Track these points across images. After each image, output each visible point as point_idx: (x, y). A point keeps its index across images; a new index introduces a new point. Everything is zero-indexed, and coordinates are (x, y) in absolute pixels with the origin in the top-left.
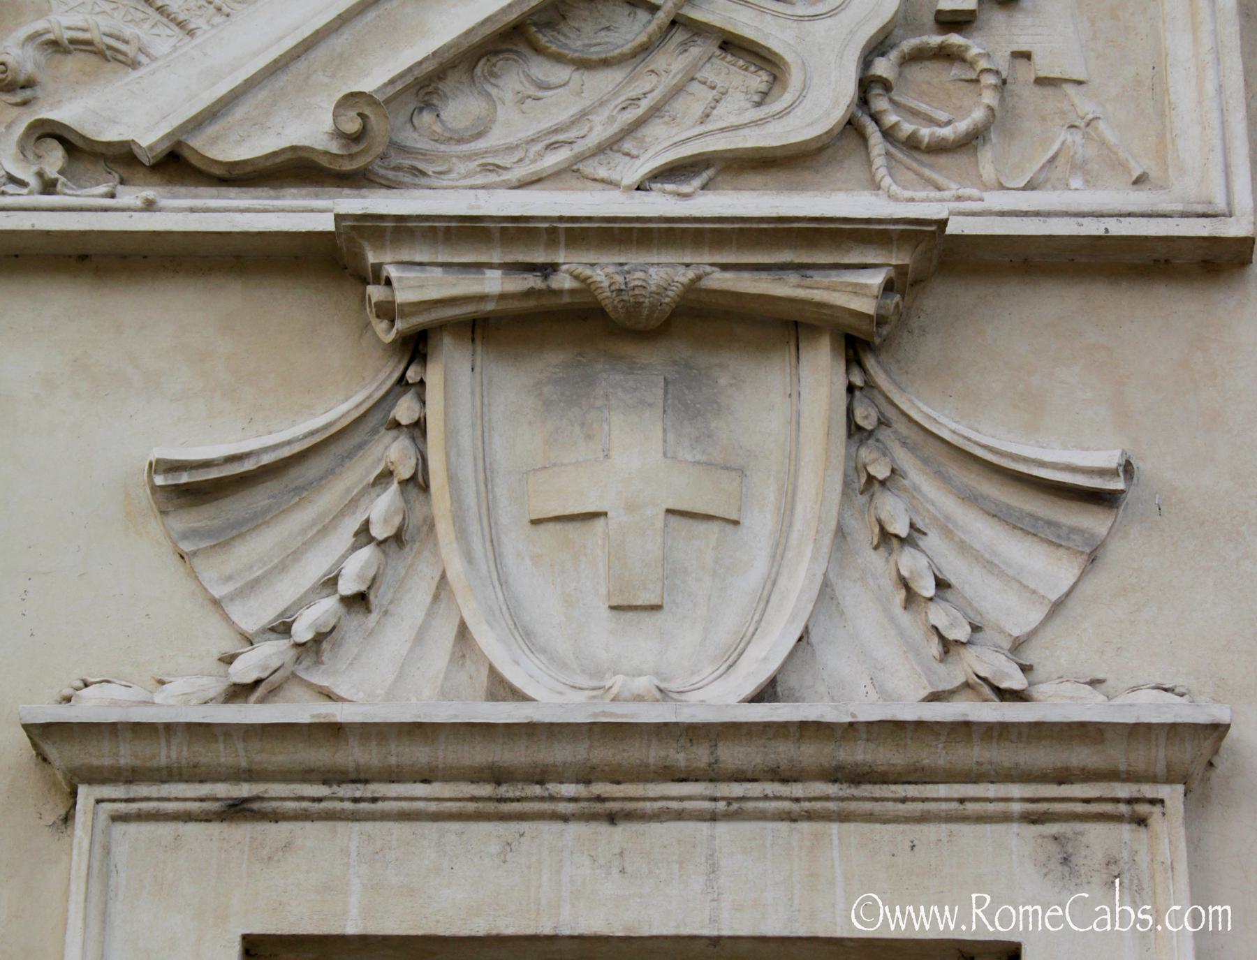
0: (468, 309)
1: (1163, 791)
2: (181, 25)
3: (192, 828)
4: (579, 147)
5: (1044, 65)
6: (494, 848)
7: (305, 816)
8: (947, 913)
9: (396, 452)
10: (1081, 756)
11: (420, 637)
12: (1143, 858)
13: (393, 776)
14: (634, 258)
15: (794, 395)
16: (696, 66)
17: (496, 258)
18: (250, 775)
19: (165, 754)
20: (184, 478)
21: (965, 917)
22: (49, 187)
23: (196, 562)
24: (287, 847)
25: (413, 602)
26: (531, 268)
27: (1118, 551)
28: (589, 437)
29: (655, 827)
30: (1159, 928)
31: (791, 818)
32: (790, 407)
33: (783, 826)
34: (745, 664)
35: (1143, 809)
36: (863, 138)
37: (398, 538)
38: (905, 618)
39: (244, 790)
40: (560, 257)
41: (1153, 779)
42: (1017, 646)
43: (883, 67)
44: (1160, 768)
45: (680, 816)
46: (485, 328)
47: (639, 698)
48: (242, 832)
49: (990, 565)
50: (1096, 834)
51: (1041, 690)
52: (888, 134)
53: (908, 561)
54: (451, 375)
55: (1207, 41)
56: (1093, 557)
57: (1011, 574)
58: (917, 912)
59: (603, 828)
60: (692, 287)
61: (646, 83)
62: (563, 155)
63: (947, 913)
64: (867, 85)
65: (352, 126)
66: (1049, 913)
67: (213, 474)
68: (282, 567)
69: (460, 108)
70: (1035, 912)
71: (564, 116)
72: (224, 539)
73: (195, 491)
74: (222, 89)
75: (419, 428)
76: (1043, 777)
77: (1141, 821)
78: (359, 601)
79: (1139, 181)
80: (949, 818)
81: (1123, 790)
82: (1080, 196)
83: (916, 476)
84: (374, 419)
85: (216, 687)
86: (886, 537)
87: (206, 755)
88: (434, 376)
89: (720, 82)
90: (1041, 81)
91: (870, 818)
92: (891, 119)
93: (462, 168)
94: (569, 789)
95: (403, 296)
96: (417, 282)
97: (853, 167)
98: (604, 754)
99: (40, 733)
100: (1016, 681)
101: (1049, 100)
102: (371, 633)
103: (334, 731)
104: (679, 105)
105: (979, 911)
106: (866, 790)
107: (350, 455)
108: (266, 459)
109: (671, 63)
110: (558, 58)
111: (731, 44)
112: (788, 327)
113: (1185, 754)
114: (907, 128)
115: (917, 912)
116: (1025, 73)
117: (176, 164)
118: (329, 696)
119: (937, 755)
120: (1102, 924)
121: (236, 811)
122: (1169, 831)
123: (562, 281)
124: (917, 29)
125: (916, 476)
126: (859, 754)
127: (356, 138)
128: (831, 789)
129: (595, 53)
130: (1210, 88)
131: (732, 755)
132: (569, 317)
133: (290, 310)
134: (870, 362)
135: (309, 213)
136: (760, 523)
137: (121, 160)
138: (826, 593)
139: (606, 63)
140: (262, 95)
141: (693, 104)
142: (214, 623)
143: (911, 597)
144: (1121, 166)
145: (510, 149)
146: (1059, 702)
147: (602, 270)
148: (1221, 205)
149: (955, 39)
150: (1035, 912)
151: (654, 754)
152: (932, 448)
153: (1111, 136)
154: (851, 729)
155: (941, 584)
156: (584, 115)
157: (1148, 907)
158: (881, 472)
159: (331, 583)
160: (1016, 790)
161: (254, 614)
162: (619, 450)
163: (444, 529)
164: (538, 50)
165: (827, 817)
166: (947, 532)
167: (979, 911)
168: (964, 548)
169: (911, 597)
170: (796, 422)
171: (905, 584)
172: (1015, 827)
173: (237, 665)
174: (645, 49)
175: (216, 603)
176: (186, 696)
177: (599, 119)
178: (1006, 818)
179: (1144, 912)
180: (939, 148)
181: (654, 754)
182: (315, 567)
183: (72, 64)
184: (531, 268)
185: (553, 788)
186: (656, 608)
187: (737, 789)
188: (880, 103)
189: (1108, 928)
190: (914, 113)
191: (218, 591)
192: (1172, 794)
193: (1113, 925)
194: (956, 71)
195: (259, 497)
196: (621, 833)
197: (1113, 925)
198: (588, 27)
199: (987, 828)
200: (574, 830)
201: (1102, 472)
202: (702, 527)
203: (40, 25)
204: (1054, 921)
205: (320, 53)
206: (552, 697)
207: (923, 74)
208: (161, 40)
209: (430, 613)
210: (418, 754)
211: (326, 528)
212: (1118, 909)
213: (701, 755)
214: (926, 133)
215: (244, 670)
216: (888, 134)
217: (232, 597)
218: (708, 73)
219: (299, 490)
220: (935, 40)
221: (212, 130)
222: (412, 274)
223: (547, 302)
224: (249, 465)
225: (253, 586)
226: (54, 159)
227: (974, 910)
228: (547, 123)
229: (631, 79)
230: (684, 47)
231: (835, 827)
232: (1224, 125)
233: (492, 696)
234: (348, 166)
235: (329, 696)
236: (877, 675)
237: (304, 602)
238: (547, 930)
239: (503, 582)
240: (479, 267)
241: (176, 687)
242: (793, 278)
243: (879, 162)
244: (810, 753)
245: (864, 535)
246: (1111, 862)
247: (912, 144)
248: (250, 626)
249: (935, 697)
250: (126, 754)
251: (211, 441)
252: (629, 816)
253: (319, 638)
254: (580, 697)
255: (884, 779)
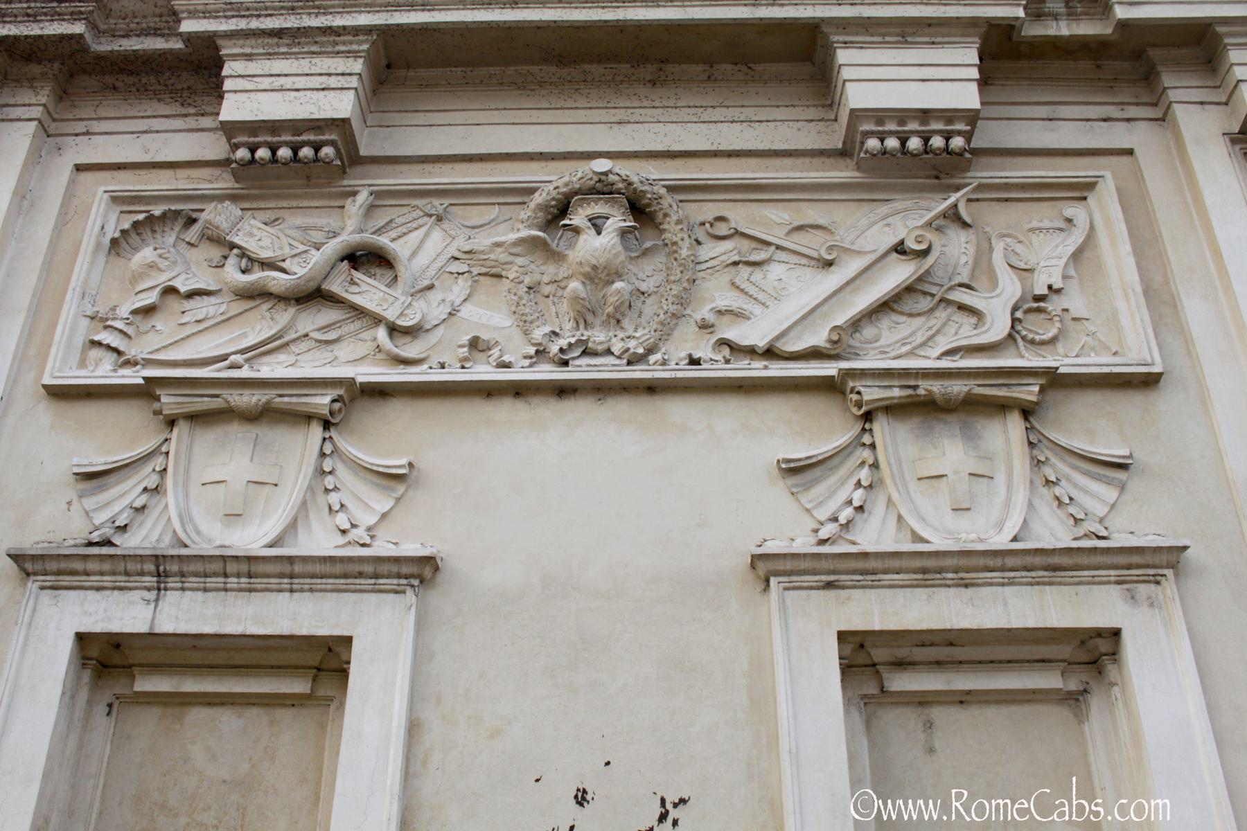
0: (888, 402)
1: (1165, 571)
2: (763, 304)
3: (812, 592)
4: (914, 344)
5: (1075, 313)
6: (925, 597)
7: (854, 587)
8: (931, 806)
9: (866, 454)
10: (1136, 559)
11: (884, 520)
12: (1161, 597)
13: (886, 572)
14: (946, 383)
15: (1005, 431)
16: (950, 315)
17: (896, 383)
18: (834, 572)
19: (803, 565)
20: (792, 465)
21: (946, 808)
22: (727, 361)
23: (799, 496)
24: (849, 598)
25: (878, 508)
26: (909, 387)
27: (1131, 485)
28: (935, 448)
29: (983, 589)
30: (1109, 818)
31: (1031, 584)
32: (1007, 435)
33: (1029, 588)
34: (1006, 529)
35: (1159, 578)
36: (1015, 340)
37: (870, 486)
38: (1058, 511)
39: (832, 578)
40: (920, 383)
41: (1162, 567)
42: (1101, 521)
43: (1019, 314)
44: (1165, 563)
45: (991, 584)
46: (892, 409)
47: (972, 541)
48: (831, 593)
49: (1086, 492)
50: (1142, 588)
51: (1115, 536)
52: (1023, 338)
53: (1057, 491)
54: (881, 428)
55: (1133, 303)
56: (1122, 487)
57: (1096, 496)
58: (906, 805)
59: (963, 590)
60: (968, 394)
61: (933, 322)
62: (907, 348)
63: (931, 806)
64: (1014, 320)
65: (835, 338)
66: (1016, 806)
67: (802, 463)
68: (830, 497)
69: (868, 332)
70: (1006, 805)
71: (906, 334)
72: (808, 486)
73: (793, 469)
74: (785, 326)
75: (873, 446)
76: (1122, 568)
77: (1158, 583)
78: (860, 509)
79: (1115, 354)
80: (1089, 583)
81: (1151, 572)
82: (1093, 359)
83: (1054, 460)
84: (857, 443)
85: (814, 541)
86: (1048, 482)
87: (817, 565)
88: (876, 426)
89: (960, 320)
90: (1074, 319)
91: (1060, 584)
92: (1024, 333)
93: (872, 352)
94: (950, 575)
95: (866, 397)
96: (872, 393)
97: (1012, 350)
98: (963, 562)
99: (756, 559)
100: (1104, 533)
101: (1077, 325)
102: (866, 520)
103: (865, 555)
104: (946, 329)
105: (958, 804)
106: (1058, 573)
107: (848, 456)
108: (820, 458)
109: (942, 314)
110: (902, 313)
111: (962, 307)
112: (1001, 407)
113: (1172, 557)
114: (1030, 336)
115: (906, 805)
116: (1067, 317)
117: (770, 353)
118: (854, 543)
119: (1084, 560)
120: (1062, 814)
121: (829, 585)
122: (1169, 586)
123: (921, 392)
124: (1027, 302)
125: (1054, 460)
126: (1056, 560)
127: (836, 342)
128: (1046, 573)
129: (914, 311)
130: (1138, 320)
131: (1010, 562)
132: (923, 405)
133: (819, 404)
134: (1031, 419)
135: (829, 369)
136: (1001, 478)
137: (751, 352)
138: (1030, 504)
139: (919, 315)
140: (799, 328)
141: (952, 328)
142: (807, 517)
143: (1060, 503)
144: (1107, 348)
145: (889, 346)
146: (1120, 540)
147: (936, 387)
148: (1150, 361)
149: (1042, 304)
150: (1006, 805)
151: (982, 561)
152: (1058, 450)
153: (1103, 338)
154: (1053, 551)
155: (1071, 499)
156: (913, 333)
157: (1100, 801)
158: (1043, 459)
159: (850, 502)
160: (1113, 572)
161: (823, 514)
162: (949, 452)
163: (888, 481)
164: (893, 310)
165: (1044, 584)
166: (1069, 480)
167: (958, 804)
168: (1076, 485)
169: (1060, 503)
170: (1008, 441)
171: (1057, 498)
172: (1112, 586)
173: (820, 533)
174: (932, 310)
175: (808, 510)
176: (804, 544)
177: (919, 334)
178: (1109, 583)
179: (1096, 805)
180: (1042, 343)
181: (982, 561)
182: (842, 496)
183: (726, 318)
184: (909, 387)
185: (944, 575)
186: (968, 509)
187: (1012, 574)
188: (1019, 327)
189: (1067, 818)
190: (1030, 331)
191: (808, 506)
192: (1169, 572)
193: (1071, 816)
194: (1043, 316)
195: (817, 472)
196: (970, 591)
197: (1071, 816)
198: (910, 302)
199: (1103, 587)
200: (952, 590)
201: (1124, 457)
202: (981, 479)
203: (713, 305)
204: (1022, 812)
205: (818, 312)
206: (939, 543)
207: (1033, 317)
208: (757, 310)
209: (886, 513)
210: (896, 563)
211: (843, 482)
212: (1075, 803)
213: (998, 562)
214: (1037, 338)
215: (824, 533)
216: (1023, 338)
217: (814, 508)
218: (954, 318)
219: (831, 469)
220: (1036, 305)
221: (783, 340)
222: (868, 390)
223: (915, 399)
224: (814, 460)
225: (820, 504)
226: (726, 351)
227: (954, 803)
228: (901, 336)
229: (928, 320)
230: (945, 309)
231: (1047, 588)
232: (1145, 333)
233: (914, 542)
234: (833, 352)
235: (854, 543)
236: (1053, 532)
237: (839, 510)
238: (949, 627)
239: (912, 501)
240: (890, 387)
241: (799, 541)
242: (1005, 389)
243: (1022, 348)
244: (1038, 560)
245: (1039, 482)
246: (1149, 598)
247: (1032, 342)
248: (822, 519)
249: (1075, 539)
250: (789, 565)
251: (800, 452)
252: (973, 585)
253: (849, 522)
254: (951, 542)
255: (1065, 569)
